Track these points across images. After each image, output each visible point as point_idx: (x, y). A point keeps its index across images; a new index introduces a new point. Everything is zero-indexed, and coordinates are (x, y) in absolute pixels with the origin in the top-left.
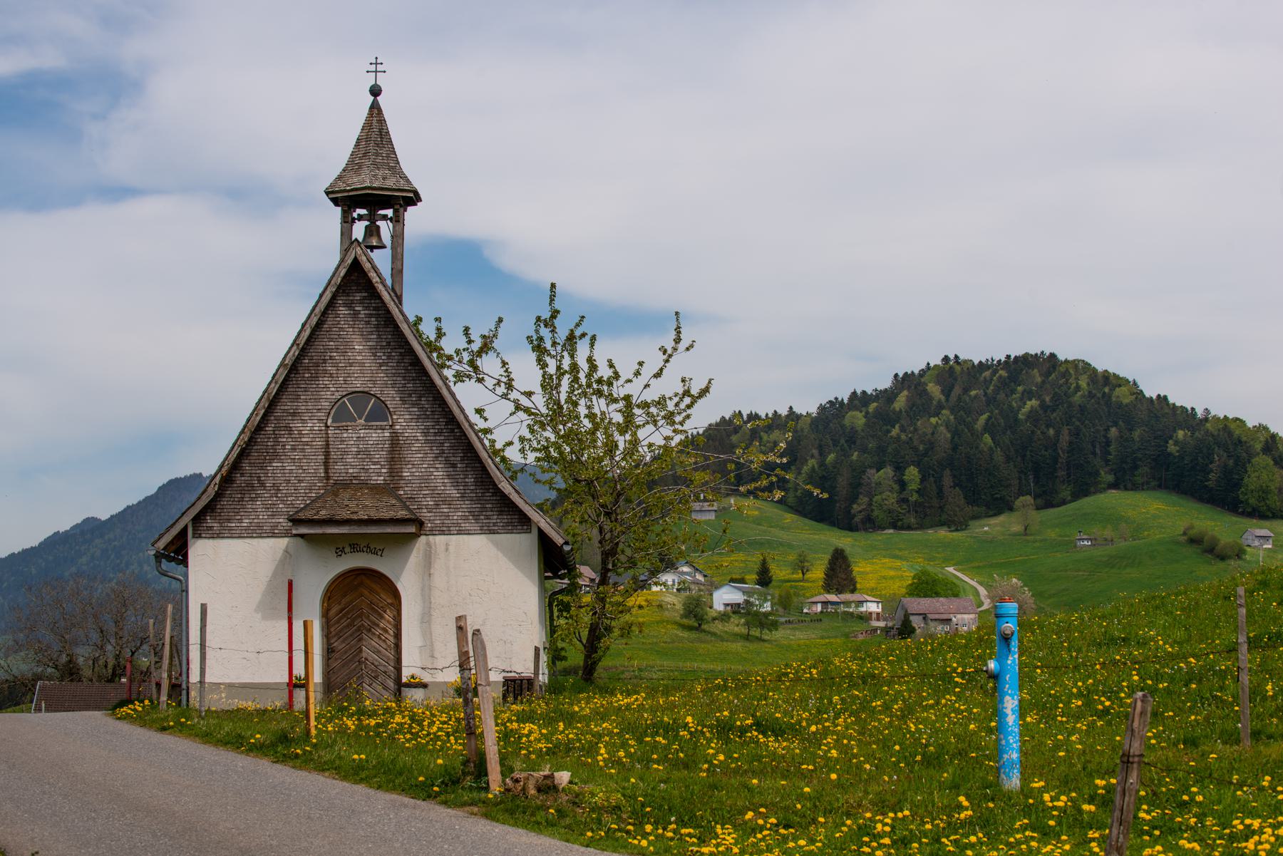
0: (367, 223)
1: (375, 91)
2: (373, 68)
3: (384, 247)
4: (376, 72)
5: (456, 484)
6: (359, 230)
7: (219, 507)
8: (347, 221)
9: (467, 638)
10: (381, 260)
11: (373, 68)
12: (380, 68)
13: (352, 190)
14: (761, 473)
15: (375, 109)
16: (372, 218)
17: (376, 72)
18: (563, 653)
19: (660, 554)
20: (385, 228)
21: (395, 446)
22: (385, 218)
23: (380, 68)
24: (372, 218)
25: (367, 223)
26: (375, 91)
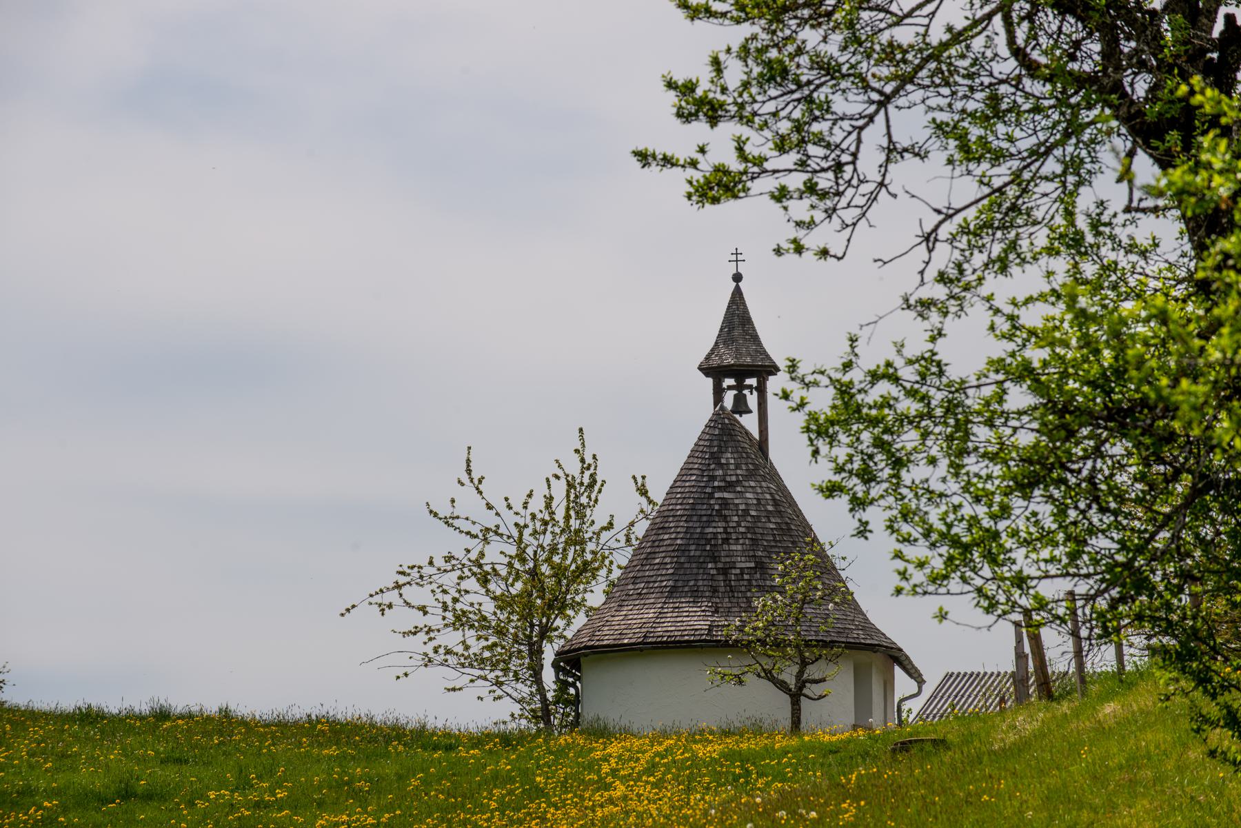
0: (735, 392)
1: (737, 278)
2: (734, 258)
3: (750, 412)
4: (737, 261)
6: (729, 400)
7: (723, 554)
8: (718, 393)
9: (1028, 636)
10: (750, 422)
11: (734, 258)
12: (740, 257)
14: (1040, 253)
15: (737, 296)
16: (740, 387)
17: (737, 261)
18: (868, 534)
19: (949, 401)
20: (752, 400)
22: (750, 387)
23: (740, 257)
24: (740, 387)
25: (735, 392)
26: (737, 278)
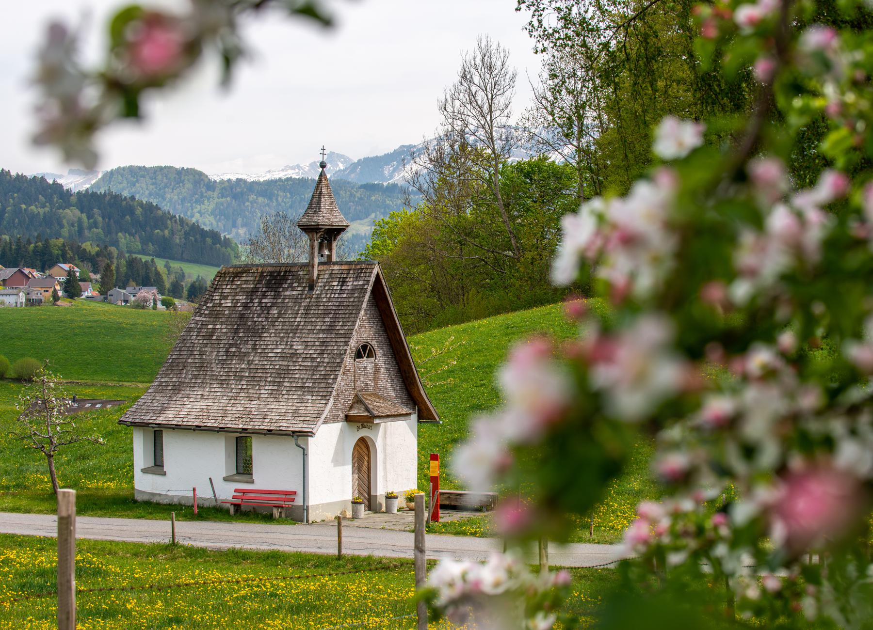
5: (394, 390)
13: (336, 226)
21: (376, 370)
